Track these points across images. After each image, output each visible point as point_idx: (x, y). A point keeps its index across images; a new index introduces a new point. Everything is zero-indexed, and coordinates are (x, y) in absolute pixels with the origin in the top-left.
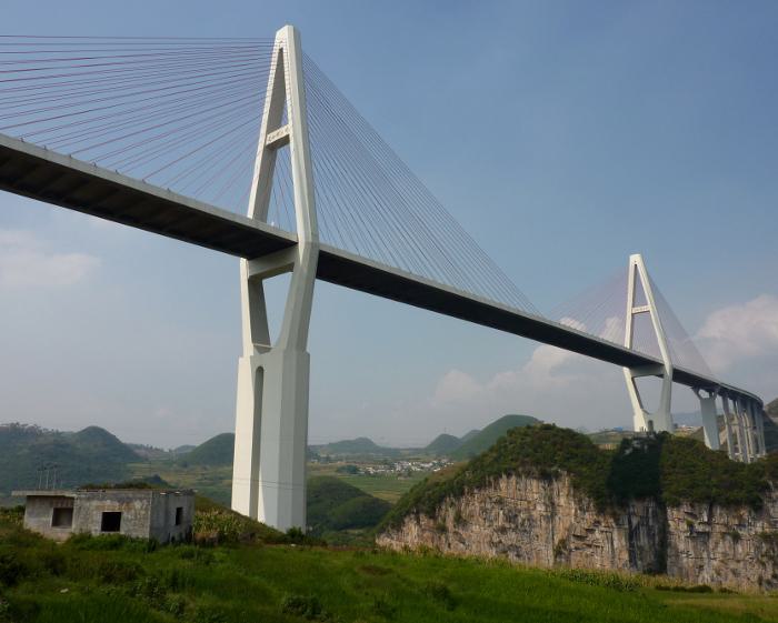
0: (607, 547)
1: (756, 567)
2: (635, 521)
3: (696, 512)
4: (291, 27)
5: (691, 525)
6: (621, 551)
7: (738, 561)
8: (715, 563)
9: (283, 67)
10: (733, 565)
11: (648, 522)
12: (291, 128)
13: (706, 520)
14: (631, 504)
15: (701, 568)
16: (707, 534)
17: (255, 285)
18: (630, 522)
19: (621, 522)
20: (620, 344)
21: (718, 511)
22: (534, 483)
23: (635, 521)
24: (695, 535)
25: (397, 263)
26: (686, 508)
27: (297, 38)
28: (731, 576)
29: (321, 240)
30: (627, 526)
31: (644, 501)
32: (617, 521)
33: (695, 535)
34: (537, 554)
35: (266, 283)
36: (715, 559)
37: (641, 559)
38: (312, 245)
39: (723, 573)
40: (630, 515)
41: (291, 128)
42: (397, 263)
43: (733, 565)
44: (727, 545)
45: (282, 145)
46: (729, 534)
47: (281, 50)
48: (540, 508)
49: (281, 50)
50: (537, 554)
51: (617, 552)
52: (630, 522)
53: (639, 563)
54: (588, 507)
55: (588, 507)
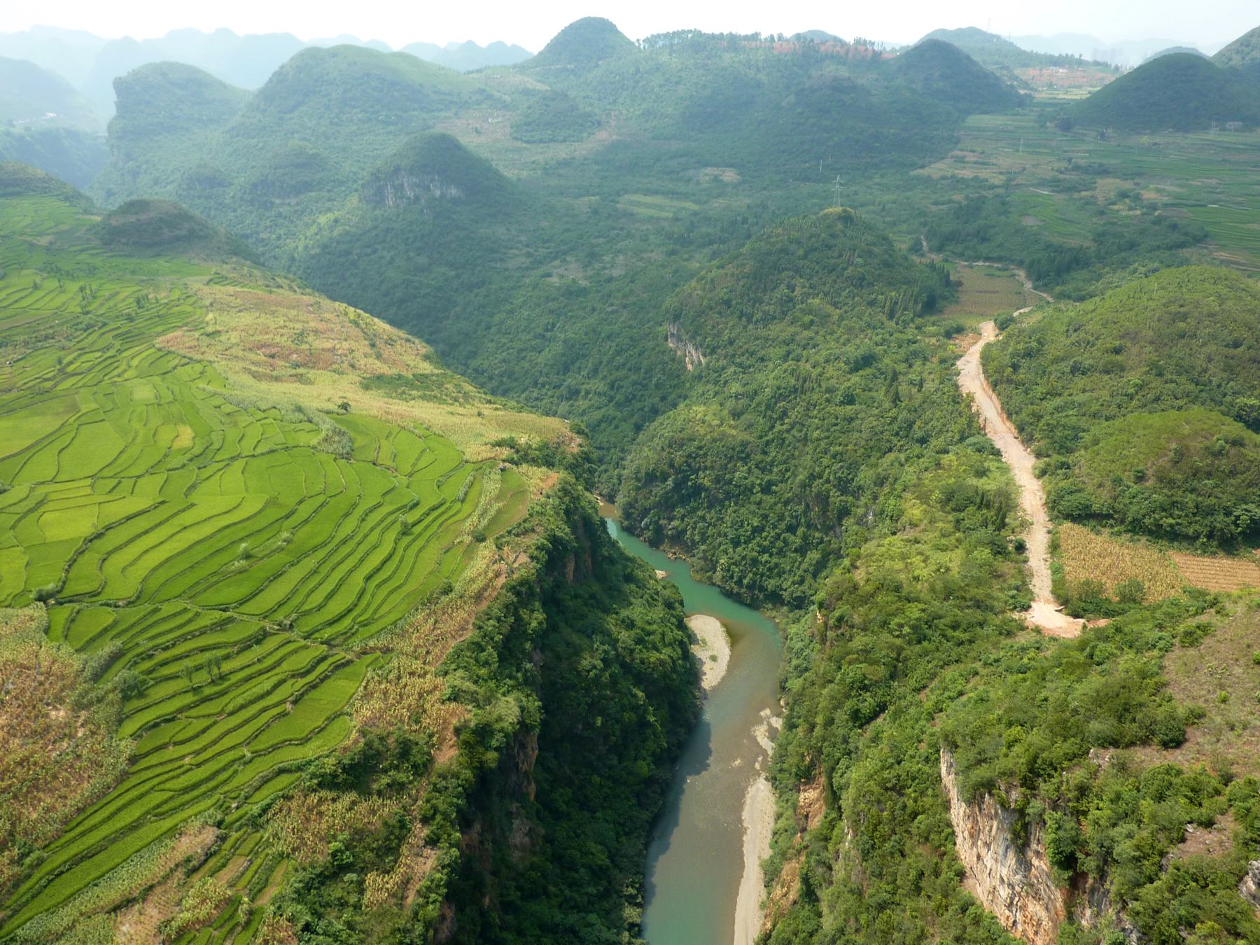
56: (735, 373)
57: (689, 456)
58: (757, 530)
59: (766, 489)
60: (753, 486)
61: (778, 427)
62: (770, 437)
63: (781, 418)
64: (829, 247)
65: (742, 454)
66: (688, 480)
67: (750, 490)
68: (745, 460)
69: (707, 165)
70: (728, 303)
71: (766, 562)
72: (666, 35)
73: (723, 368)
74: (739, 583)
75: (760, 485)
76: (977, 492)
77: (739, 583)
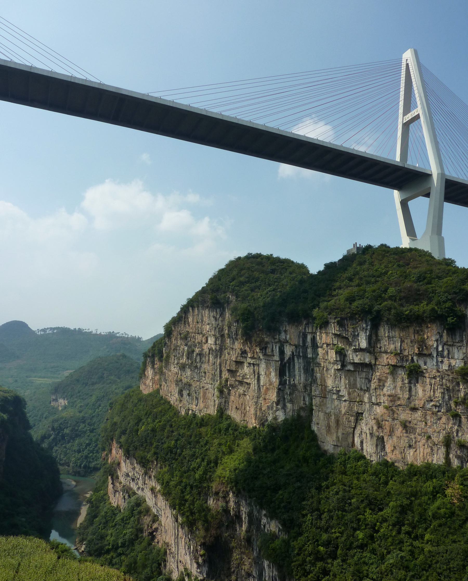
0: (254, 383)
1: (444, 420)
2: (288, 350)
3: (349, 334)
4: (413, 49)
5: (341, 353)
6: (267, 389)
7: (414, 409)
8: (379, 410)
9: (410, 72)
10: (404, 415)
11: (305, 353)
12: (419, 110)
13: (364, 344)
14: (282, 329)
15: (359, 416)
16: (370, 367)
17: (404, 204)
18: (282, 353)
19: (269, 351)
20: (389, 157)
21: (384, 331)
22: (206, 312)
23: (288, 350)
24: (351, 368)
25: (458, 175)
26: (334, 329)
27: (416, 53)
28: (399, 431)
29: (447, 173)
30: (277, 358)
31: (300, 323)
32: (264, 349)
33: (351, 368)
34: (205, 394)
35: (410, 203)
36: (378, 404)
37: (291, 401)
38: (442, 175)
39: (387, 425)
40: (282, 344)
41: (419, 110)
42: (458, 175)
43: (404, 415)
44: (399, 384)
45: (417, 120)
46: (402, 367)
47: (407, 65)
48: (211, 341)
49: (407, 65)
50: (205, 394)
51: (263, 390)
52: (282, 353)
53: (289, 405)
54: (237, 334)
55: (237, 334)
56: (80, 402)
57: (61, 424)
58: (88, 445)
59: (92, 431)
60: (86, 430)
61: (97, 410)
62: (94, 414)
63: (98, 408)
64: (117, 362)
65: (83, 420)
66: (60, 433)
67: (85, 432)
68: (84, 422)
69: (67, 370)
70: (78, 381)
71: (91, 456)
72: (51, 329)
73: (75, 401)
74: (80, 466)
75: (89, 430)
76: (142, 525)
77: (80, 466)
